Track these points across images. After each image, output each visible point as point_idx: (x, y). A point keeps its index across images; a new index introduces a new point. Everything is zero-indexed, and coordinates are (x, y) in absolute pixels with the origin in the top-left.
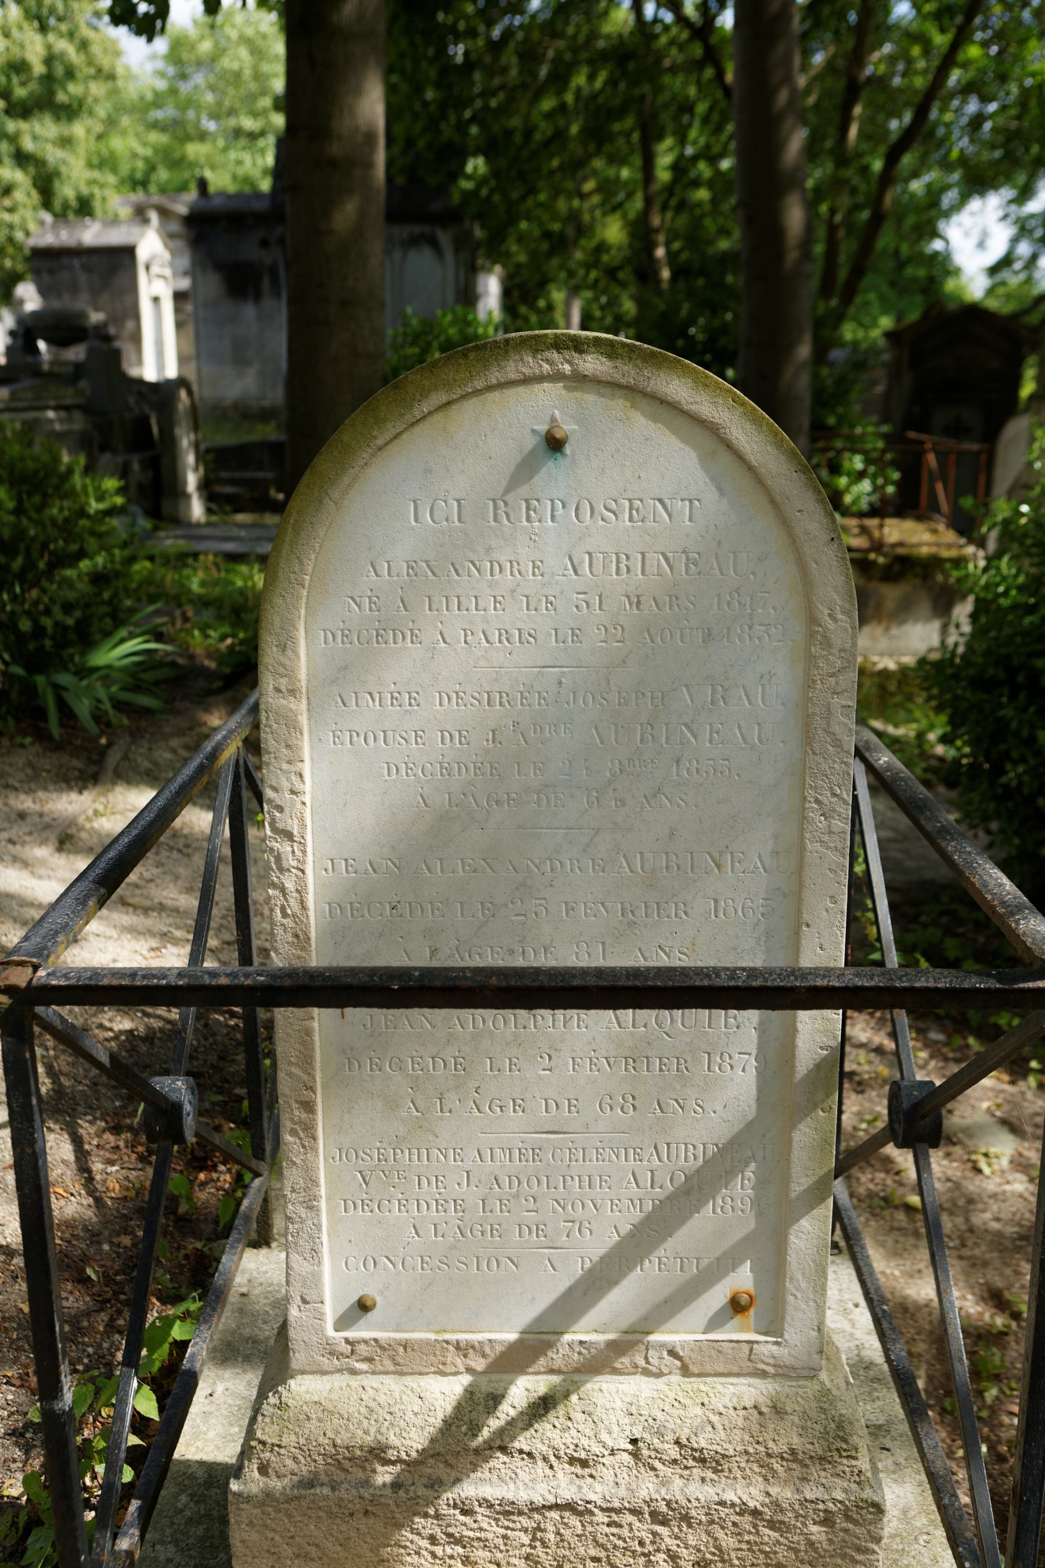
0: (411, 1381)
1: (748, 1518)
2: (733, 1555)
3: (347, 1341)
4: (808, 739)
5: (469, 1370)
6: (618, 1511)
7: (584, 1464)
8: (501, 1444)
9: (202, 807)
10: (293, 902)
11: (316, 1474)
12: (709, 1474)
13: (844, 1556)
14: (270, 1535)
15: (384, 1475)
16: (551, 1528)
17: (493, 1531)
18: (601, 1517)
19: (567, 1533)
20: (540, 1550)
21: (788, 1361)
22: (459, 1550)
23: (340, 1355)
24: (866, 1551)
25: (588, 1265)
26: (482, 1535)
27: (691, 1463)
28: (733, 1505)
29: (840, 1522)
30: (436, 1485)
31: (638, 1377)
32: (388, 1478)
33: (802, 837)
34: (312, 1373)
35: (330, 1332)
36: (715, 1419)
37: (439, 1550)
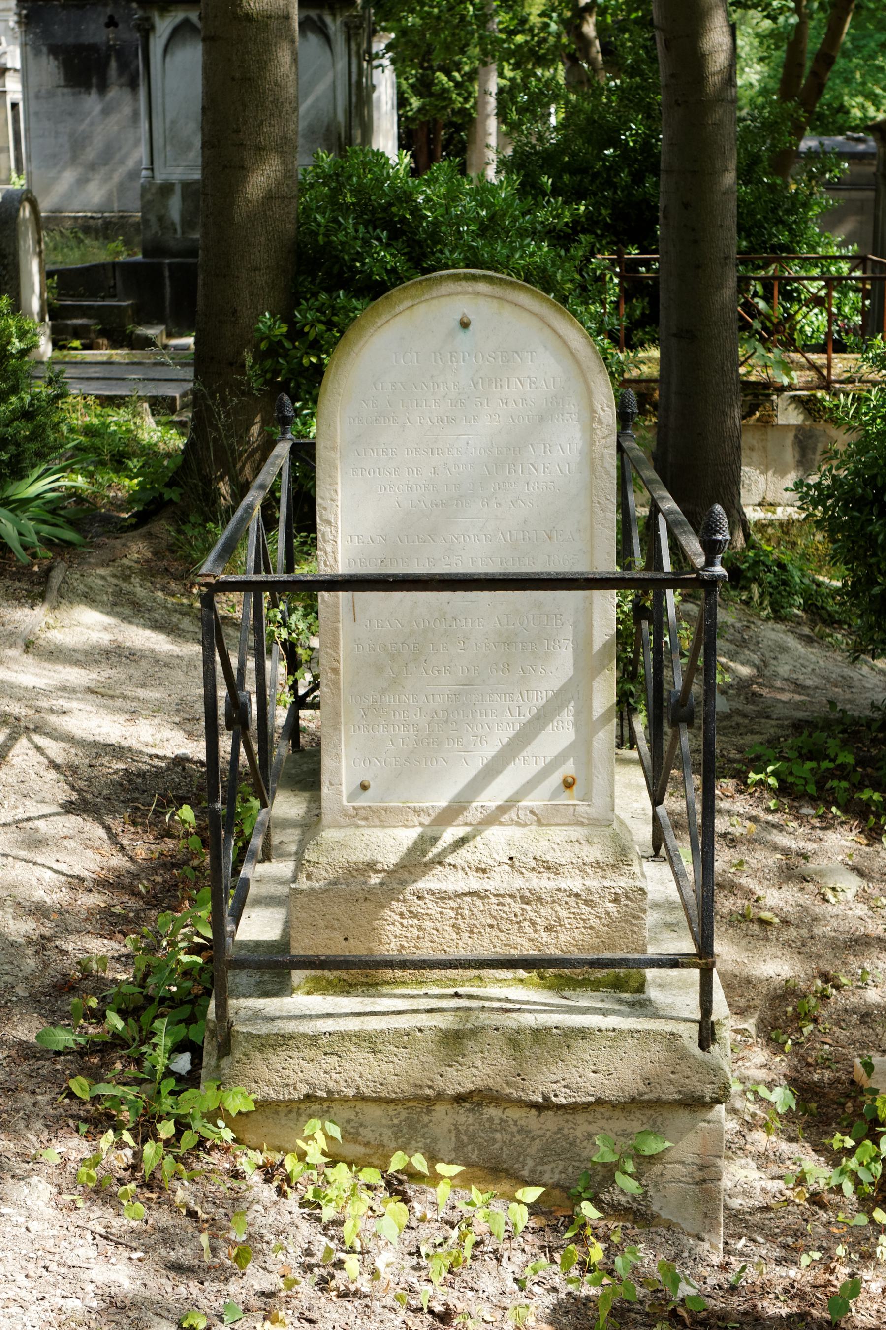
0: (389, 831)
1: (573, 899)
2: (566, 921)
3: (354, 808)
4: (593, 471)
5: (421, 824)
6: (503, 896)
7: (484, 871)
8: (439, 861)
9: (137, 625)
10: (330, 558)
11: (338, 879)
12: (552, 876)
13: (626, 921)
14: (312, 914)
15: (375, 879)
16: (466, 907)
17: (434, 910)
18: (493, 900)
19: (475, 910)
20: (460, 921)
21: (595, 816)
22: (416, 921)
23: (350, 817)
24: (638, 918)
25: (485, 762)
26: (429, 912)
27: (542, 870)
28: (565, 891)
29: (624, 901)
30: (404, 883)
31: (513, 827)
32: (377, 881)
33: (592, 521)
34: (335, 827)
35: (345, 803)
36: (555, 847)
37: (405, 922)
